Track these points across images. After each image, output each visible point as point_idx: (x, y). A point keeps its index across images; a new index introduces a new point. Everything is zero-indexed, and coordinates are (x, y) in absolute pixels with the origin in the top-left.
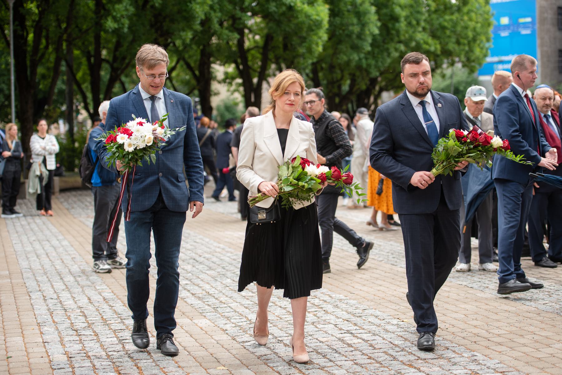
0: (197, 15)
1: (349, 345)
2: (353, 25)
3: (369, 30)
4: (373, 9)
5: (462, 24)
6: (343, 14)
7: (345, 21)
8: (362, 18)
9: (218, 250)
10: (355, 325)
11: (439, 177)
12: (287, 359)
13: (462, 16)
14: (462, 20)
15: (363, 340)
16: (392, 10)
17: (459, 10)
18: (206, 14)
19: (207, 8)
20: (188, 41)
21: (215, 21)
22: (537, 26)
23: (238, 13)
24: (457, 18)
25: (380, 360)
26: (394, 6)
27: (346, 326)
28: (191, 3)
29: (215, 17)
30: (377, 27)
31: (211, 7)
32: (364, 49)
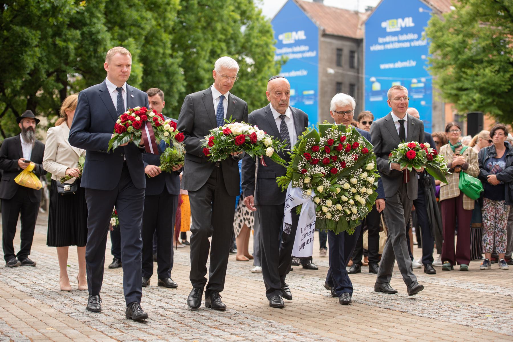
0: (27, 66)
1: (162, 315)
2: (163, 83)
3: (177, 88)
4: (181, 71)
5: (257, 89)
6: (155, 74)
7: (156, 79)
8: (171, 78)
9: (42, 257)
10: (167, 303)
11: (163, 173)
12: (109, 324)
13: (257, 82)
14: (257, 85)
15: (175, 312)
16: (197, 73)
17: (254, 76)
18: (35, 66)
19: (36, 60)
20: (18, 88)
21: (43, 72)
22: (319, 98)
23: (64, 67)
24: (252, 83)
25: (189, 324)
26: (199, 69)
27: (159, 304)
28: (22, 54)
29: (43, 68)
30: (183, 86)
31: (40, 59)
32: (172, 104)
